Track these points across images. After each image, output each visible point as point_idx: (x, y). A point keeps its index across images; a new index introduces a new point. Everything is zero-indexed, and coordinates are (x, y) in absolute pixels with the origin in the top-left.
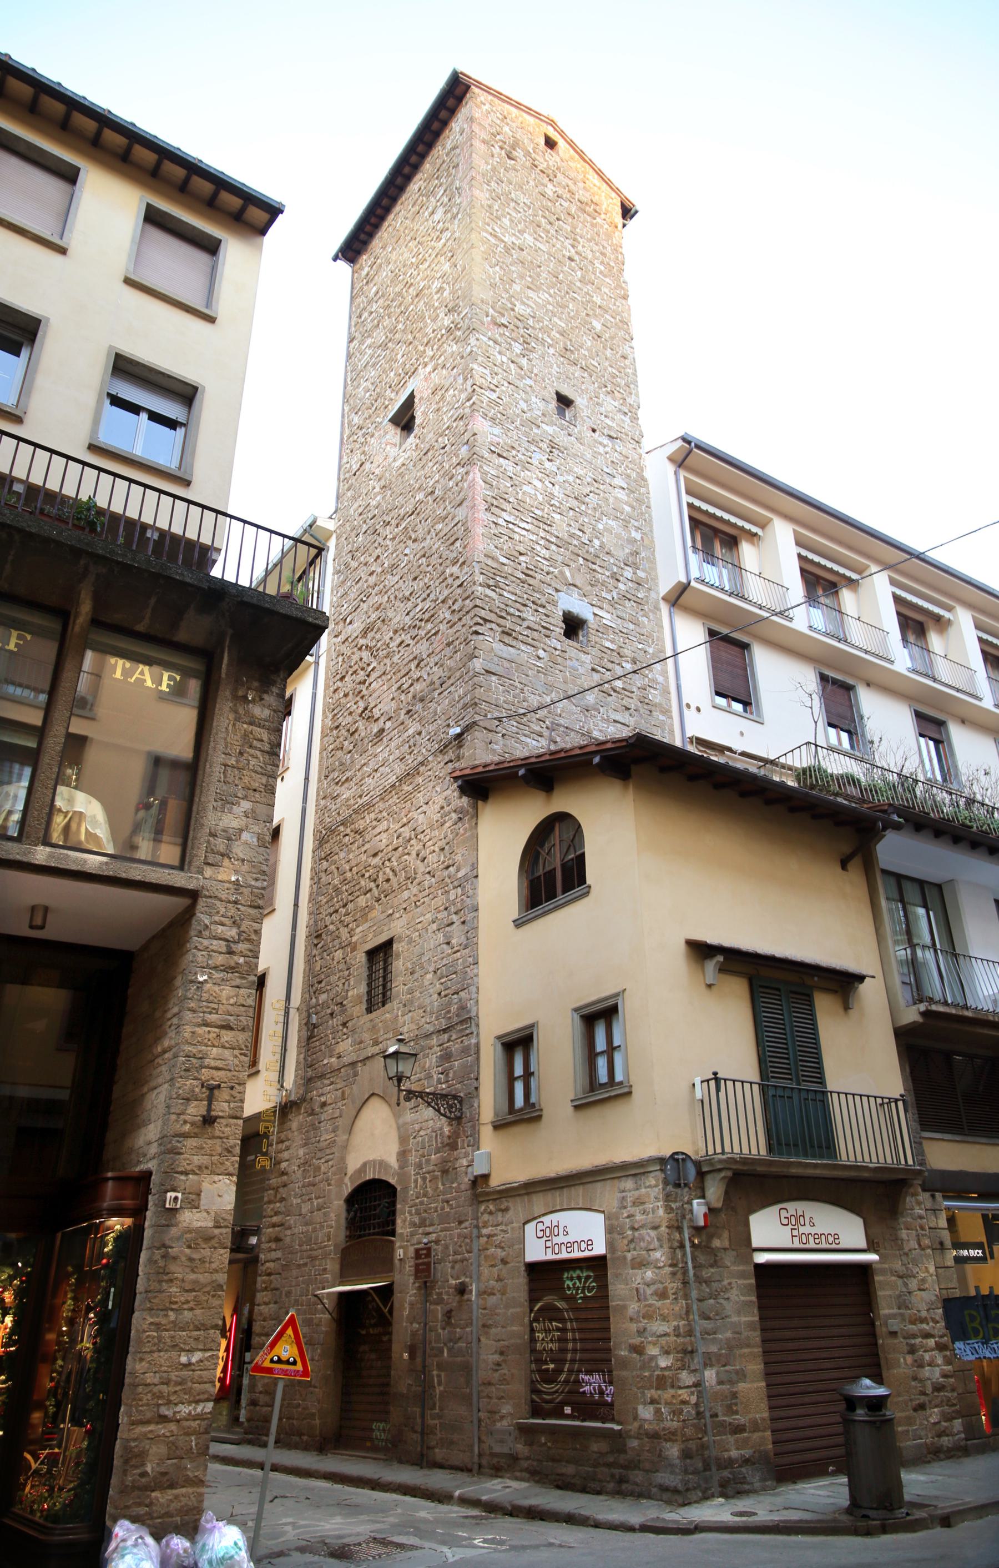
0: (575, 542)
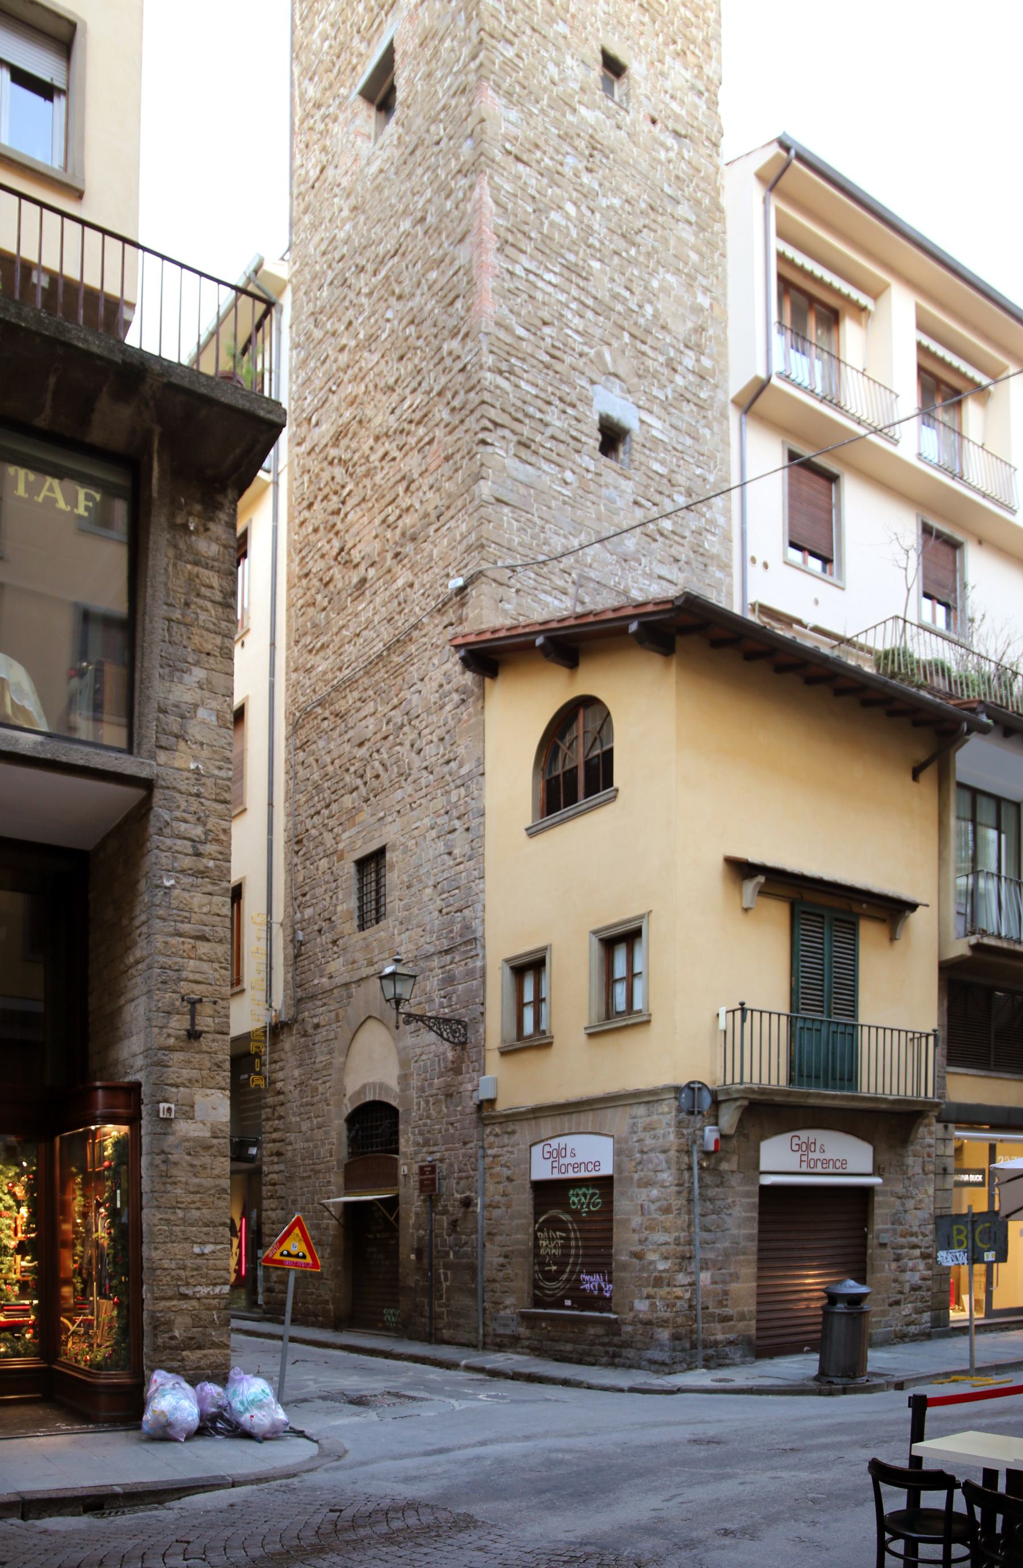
0: (619, 308)
